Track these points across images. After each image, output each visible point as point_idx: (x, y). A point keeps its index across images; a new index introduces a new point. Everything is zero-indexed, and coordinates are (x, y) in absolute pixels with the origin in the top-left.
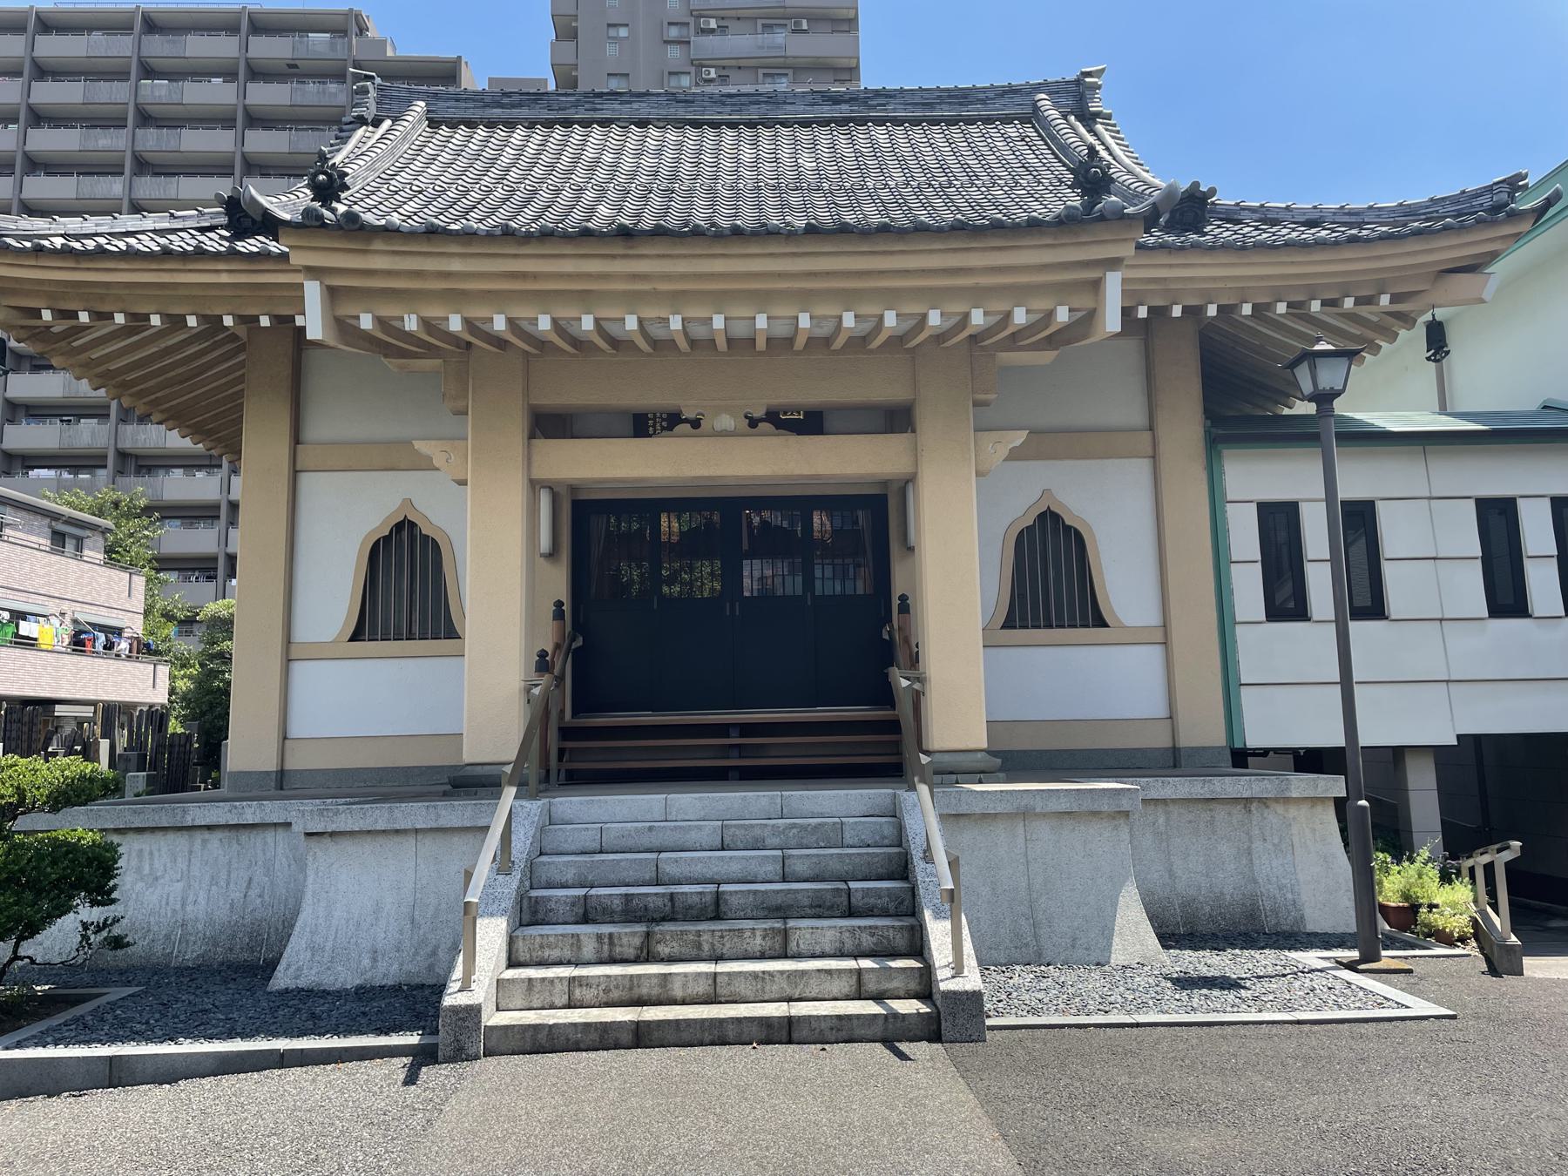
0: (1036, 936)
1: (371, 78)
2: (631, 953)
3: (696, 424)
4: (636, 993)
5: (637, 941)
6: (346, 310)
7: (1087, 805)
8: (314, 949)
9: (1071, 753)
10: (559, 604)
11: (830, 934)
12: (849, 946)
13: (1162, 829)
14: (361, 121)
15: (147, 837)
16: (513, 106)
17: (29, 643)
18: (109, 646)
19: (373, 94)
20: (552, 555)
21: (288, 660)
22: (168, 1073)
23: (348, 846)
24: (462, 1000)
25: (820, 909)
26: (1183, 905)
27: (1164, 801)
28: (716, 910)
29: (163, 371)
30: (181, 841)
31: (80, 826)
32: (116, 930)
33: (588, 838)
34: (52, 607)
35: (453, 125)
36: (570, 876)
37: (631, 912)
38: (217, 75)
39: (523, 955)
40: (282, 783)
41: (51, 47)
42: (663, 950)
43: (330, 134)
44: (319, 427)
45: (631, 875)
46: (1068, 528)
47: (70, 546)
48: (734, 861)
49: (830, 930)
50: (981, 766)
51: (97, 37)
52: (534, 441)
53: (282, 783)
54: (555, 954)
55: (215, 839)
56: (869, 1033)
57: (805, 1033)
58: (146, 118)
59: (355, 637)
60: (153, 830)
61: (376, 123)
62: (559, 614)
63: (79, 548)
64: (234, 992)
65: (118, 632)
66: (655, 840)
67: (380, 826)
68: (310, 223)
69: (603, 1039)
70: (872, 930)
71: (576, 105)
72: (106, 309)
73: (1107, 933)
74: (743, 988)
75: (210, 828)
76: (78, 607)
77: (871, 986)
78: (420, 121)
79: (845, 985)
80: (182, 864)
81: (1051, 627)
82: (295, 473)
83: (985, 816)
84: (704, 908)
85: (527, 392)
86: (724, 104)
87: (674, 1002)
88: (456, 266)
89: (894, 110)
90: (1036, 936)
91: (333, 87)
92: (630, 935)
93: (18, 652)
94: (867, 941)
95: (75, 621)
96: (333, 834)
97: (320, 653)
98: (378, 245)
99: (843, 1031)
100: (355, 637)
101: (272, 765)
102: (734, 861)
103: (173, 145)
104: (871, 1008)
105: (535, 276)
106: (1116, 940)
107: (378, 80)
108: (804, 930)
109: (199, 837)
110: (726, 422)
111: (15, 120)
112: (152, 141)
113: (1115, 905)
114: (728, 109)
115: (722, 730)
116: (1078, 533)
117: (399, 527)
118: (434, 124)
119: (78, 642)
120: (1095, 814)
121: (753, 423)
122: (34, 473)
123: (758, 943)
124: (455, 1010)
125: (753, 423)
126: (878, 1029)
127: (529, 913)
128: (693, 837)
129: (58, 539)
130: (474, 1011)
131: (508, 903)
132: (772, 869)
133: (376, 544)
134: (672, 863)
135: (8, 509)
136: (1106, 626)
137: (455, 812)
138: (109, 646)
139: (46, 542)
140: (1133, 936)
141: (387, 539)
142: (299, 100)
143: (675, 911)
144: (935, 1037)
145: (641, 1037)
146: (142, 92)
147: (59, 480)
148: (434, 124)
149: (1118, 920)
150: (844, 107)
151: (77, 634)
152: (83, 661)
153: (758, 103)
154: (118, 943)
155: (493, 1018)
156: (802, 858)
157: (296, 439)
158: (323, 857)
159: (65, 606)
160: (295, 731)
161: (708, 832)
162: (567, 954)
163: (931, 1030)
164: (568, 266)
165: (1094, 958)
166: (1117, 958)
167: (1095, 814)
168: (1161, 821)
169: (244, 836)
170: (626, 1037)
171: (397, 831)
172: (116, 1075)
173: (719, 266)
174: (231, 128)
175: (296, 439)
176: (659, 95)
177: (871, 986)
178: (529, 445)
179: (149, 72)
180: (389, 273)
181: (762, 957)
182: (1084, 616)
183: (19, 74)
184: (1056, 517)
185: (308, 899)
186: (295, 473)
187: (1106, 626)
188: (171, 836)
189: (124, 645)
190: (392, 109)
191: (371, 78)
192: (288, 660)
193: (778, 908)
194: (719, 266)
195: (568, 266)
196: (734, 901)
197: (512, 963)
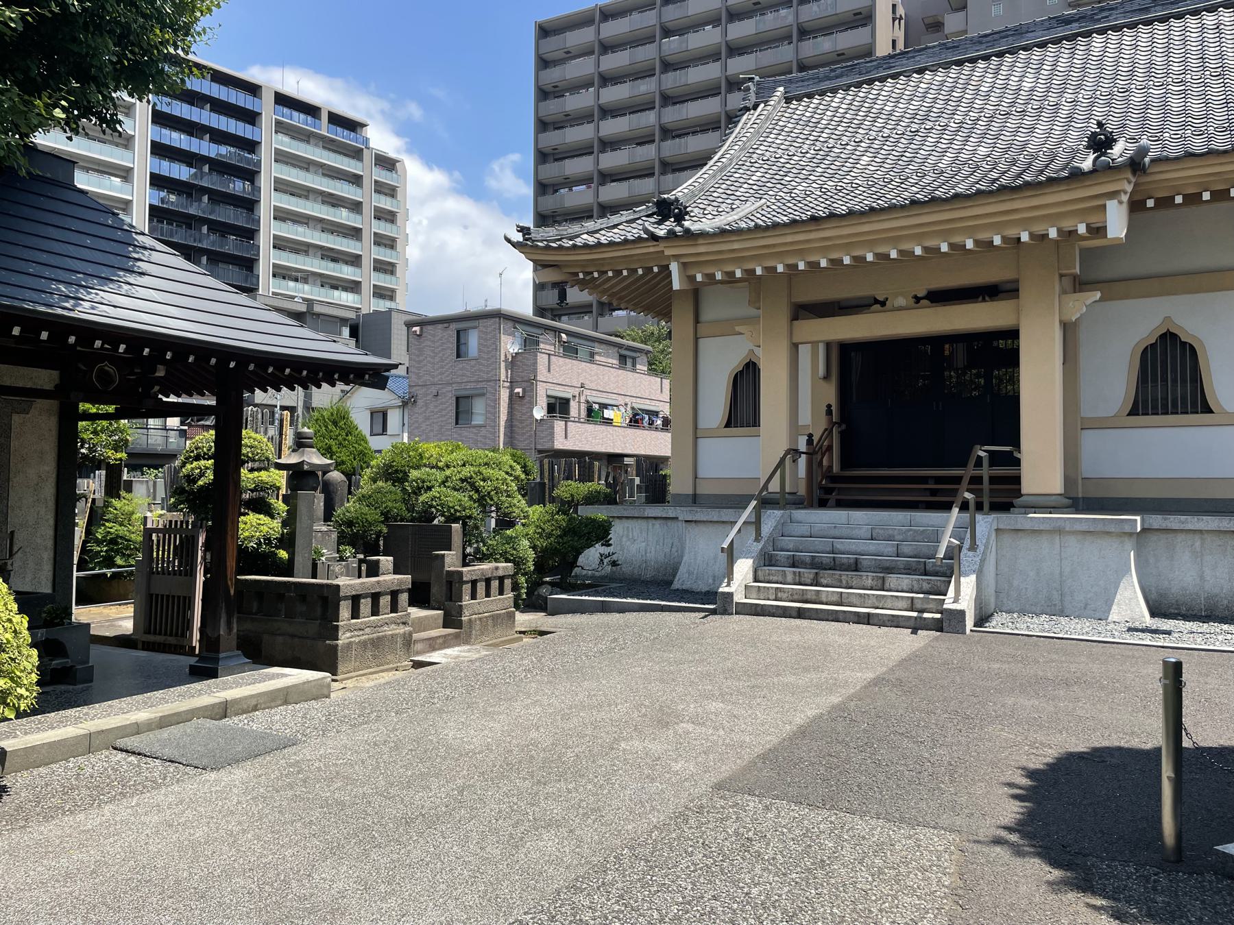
0: (1061, 601)
1: (751, 79)
2: (809, 581)
3: (883, 304)
4: (805, 597)
5: (812, 576)
6: (691, 272)
7: (1100, 527)
8: (690, 573)
9: (1179, 500)
10: (829, 406)
11: (906, 581)
12: (916, 588)
13: (1198, 549)
14: (747, 109)
15: (630, 521)
16: (837, 77)
17: (608, 422)
18: (651, 423)
19: (753, 88)
20: (827, 377)
21: (696, 438)
22: (622, 609)
23: (703, 528)
24: (727, 590)
25: (909, 570)
26: (1207, 599)
27: (1201, 531)
28: (856, 567)
29: (637, 289)
30: (643, 523)
31: (600, 513)
32: (615, 557)
33: (804, 529)
34: (621, 400)
35: (799, 99)
36: (791, 546)
37: (816, 565)
38: (707, 24)
39: (761, 578)
40: (695, 499)
41: (611, 29)
42: (824, 581)
43: (715, 135)
44: (708, 314)
45: (820, 548)
46: (1184, 344)
47: (629, 362)
48: (872, 546)
49: (906, 580)
50: (1053, 504)
51: (636, 16)
52: (795, 322)
53: (695, 499)
54: (775, 578)
55: (657, 523)
56: (907, 624)
57: (876, 621)
58: (667, 66)
59: (728, 425)
60: (627, 518)
61: (755, 107)
62: (829, 411)
63: (634, 365)
64: (659, 587)
65: (656, 414)
66: (837, 533)
67: (715, 519)
68: (671, 234)
69: (785, 613)
70: (929, 582)
71: (877, 67)
72: (605, 269)
73: (1109, 604)
74: (854, 600)
75: (655, 518)
76: (634, 400)
77: (918, 605)
78: (779, 102)
79: (904, 604)
80: (644, 534)
81: (1167, 413)
82: (696, 339)
83: (1034, 531)
84: (849, 566)
85: (790, 295)
86: (981, 43)
87: (822, 603)
88: (736, 246)
89: (1116, 19)
90: (1061, 601)
91: (783, 12)
92: (808, 574)
93: (603, 427)
94: (926, 586)
95: (633, 408)
96: (696, 522)
97: (711, 434)
98: (701, 241)
99: (895, 622)
100: (728, 425)
101: (690, 492)
102: (872, 546)
103: (683, 82)
104: (915, 614)
105: (774, 246)
106: (1114, 607)
107: (757, 78)
108: (892, 580)
109: (651, 522)
110: (901, 301)
111: (592, 85)
112: (672, 81)
113: (1117, 588)
114: (984, 46)
115: (924, 480)
116: (1191, 347)
117: (747, 365)
118: (788, 100)
119: (634, 422)
120: (1108, 533)
121: (917, 299)
122: (616, 313)
123: (869, 582)
124: (723, 593)
125: (917, 299)
126: (912, 623)
127: (766, 560)
128: (856, 533)
129: (623, 359)
130: (730, 595)
131: (754, 554)
132: (892, 550)
133: (736, 375)
134: (839, 545)
135: (596, 344)
136: (1211, 412)
137: (726, 514)
138: (651, 423)
139: (616, 362)
140: (1130, 604)
141: (741, 372)
142: (762, 28)
143: (835, 566)
144: (940, 630)
145: (800, 614)
146: (664, 48)
147: (629, 316)
148: (788, 100)
149: (1118, 596)
150: (1075, 25)
151: (635, 415)
152: (638, 432)
153: (1007, 36)
154: (614, 564)
155: (739, 598)
156: (906, 548)
157: (697, 321)
158: (694, 531)
159: (628, 400)
160: (700, 475)
161: (865, 531)
162: (780, 579)
163: (938, 626)
164: (789, 239)
165: (1098, 615)
166: (1113, 616)
167: (1108, 533)
168: (1198, 544)
169: (669, 523)
170: (794, 614)
171: (723, 522)
172: (604, 608)
173: (866, 228)
174: (718, 60)
175: (697, 321)
176: (934, 47)
177: (918, 605)
178: (791, 325)
179: (667, 32)
180: (707, 253)
181: (871, 589)
182: (1194, 404)
183: (592, 53)
184: (1174, 336)
185: (687, 551)
186: (696, 339)
187: (1211, 412)
188: (640, 521)
189: (659, 422)
190: (764, 95)
191: (751, 79)
192: (696, 438)
193: (887, 568)
194: (866, 228)
195: (789, 239)
196: (865, 563)
197: (756, 580)
